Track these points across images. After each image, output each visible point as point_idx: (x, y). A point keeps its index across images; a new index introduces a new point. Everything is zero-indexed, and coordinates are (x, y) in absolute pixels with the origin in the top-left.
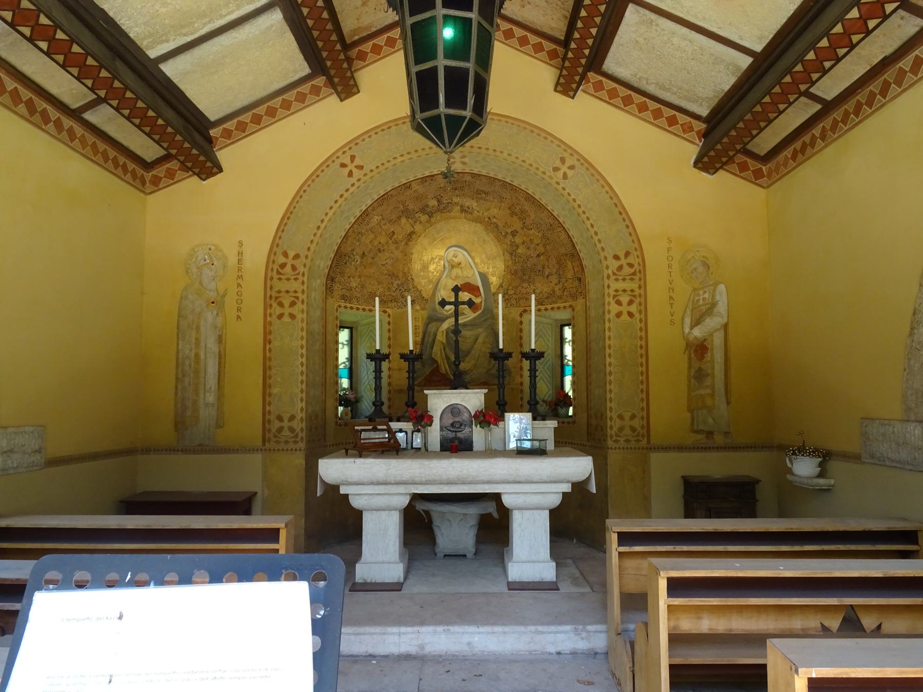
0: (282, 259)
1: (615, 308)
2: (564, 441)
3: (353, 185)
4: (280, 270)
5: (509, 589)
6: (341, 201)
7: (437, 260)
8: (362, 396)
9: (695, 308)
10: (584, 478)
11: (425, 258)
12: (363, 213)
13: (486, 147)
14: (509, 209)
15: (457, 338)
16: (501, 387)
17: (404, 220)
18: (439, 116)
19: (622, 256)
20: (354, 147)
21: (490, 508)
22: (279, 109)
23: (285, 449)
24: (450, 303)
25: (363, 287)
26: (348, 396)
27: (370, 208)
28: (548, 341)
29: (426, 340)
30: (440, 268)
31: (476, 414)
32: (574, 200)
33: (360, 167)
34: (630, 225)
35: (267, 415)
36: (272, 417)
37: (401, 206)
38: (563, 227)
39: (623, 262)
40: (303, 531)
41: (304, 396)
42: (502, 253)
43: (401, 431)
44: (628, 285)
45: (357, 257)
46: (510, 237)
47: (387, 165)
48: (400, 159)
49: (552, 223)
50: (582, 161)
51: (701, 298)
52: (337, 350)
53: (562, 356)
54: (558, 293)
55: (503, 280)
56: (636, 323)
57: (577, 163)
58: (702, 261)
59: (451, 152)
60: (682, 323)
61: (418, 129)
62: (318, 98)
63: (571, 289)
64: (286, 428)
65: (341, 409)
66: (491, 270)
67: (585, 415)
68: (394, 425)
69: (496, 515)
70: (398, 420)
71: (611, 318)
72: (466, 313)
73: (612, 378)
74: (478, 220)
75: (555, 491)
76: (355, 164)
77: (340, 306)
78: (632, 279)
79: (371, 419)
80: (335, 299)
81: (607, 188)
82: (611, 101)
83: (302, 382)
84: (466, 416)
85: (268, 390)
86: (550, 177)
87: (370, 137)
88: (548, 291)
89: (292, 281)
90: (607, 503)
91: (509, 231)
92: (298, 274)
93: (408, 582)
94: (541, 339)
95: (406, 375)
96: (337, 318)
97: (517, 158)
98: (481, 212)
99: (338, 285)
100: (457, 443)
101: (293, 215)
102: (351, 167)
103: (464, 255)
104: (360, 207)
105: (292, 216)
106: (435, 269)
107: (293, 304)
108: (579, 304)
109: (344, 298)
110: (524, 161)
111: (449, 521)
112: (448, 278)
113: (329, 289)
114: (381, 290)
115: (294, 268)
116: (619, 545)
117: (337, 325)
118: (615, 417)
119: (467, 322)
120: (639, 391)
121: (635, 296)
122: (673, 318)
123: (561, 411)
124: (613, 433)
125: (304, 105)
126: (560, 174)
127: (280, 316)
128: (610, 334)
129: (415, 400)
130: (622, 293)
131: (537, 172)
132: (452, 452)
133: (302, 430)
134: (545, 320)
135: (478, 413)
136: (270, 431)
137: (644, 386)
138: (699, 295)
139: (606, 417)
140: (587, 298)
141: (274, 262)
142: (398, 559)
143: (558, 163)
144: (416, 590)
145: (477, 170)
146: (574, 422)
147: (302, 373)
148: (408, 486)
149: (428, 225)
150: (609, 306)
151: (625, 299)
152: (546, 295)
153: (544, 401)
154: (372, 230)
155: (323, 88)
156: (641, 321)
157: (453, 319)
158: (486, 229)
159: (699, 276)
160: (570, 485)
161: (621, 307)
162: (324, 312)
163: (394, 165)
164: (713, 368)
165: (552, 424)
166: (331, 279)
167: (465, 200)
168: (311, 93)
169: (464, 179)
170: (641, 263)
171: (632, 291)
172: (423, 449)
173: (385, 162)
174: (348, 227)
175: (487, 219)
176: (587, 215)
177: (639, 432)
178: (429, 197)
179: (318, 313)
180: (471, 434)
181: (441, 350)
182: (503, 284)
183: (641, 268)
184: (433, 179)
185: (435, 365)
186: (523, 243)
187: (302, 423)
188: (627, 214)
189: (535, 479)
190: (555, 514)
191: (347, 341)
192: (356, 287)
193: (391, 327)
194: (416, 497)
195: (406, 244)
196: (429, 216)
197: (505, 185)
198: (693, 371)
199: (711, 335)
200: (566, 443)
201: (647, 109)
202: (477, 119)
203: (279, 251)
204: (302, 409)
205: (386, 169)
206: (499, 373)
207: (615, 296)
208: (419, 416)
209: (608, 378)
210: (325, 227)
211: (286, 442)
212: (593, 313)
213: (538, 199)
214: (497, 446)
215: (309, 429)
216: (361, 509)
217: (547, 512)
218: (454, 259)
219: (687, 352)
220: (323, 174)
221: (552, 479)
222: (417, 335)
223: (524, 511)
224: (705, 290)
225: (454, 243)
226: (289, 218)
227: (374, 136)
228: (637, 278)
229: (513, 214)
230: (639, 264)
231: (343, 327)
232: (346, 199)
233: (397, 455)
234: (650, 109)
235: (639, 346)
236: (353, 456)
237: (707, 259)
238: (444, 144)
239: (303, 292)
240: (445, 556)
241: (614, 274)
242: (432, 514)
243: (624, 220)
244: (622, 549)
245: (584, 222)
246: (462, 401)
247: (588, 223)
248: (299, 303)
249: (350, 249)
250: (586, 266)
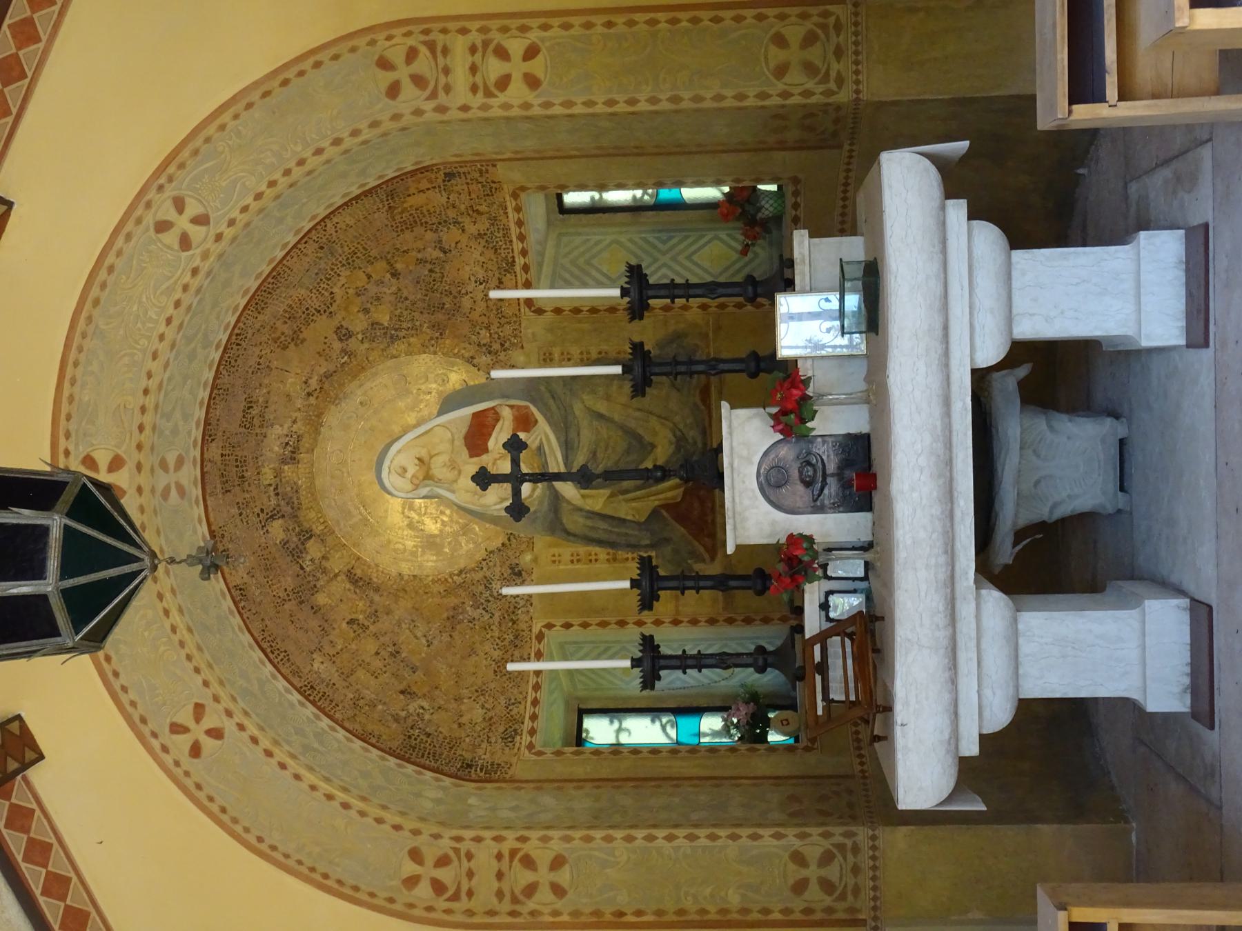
0: (424, 891)
1: (517, 92)
2: (841, 203)
3: (241, 727)
4: (450, 893)
5: (1206, 345)
6: (280, 755)
7: (413, 515)
8: (742, 686)
10: (933, 170)
11: (410, 544)
12: (307, 698)
13: (137, 411)
14: (285, 348)
15: (598, 476)
16: (714, 366)
17: (321, 599)
18: (66, 594)
19: (387, 77)
20: (152, 725)
21: (1007, 386)
22: (68, 902)
23: (871, 873)
24: (516, 493)
25: (481, 692)
26: (744, 721)
27: (296, 681)
28: (597, 244)
29: (604, 536)
30: (432, 505)
31: (781, 432)
32: (259, 196)
33: (199, 710)
34: (312, 59)
35: (792, 917)
36: (798, 904)
37: (287, 606)
38: (323, 220)
39: (403, 73)
40: (1068, 828)
41: (744, 832)
42: (390, 363)
43: (825, 606)
44: (460, 61)
45: (413, 707)
46: (353, 344)
47: (191, 648)
48: (176, 617)
49: (316, 245)
50: (162, 180)
52: (636, 750)
53: (635, 209)
54: (483, 225)
55: (455, 355)
57: (170, 192)
59: (153, 555)
61: (97, 639)
62: (38, 813)
63: (473, 196)
64: (823, 872)
65: (774, 737)
66: (434, 386)
67: (778, 155)
68: (813, 623)
69: (1023, 371)
70: (799, 611)
71: (540, 101)
72: (537, 443)
73: (686, 95)
74: (315, 422)
75: (965, 238)
76: (190, 723)
77: (530, 747)
78: (445, 51)
79: (799, 676)
80: (514, 760)
81: (226, 117)
82: (14, 111)
83: (713, 837)
84: (787, 453)
85: (736, 916)
86: (205, 256)
87: (124, 689)
88: (480, 248)
89: (473, 864)
90: (990, 100)
91: (337, 345)
92: (457, 851)
93: (1190, 587)
94: (595, 262)
95: (690, 593)
96: (558, 753)
97: (162, 337)
98: (294, 415)
99: (480, 752)
100: (851, 474)
101: (317, 866)
102: (198, 732)
103: (399, 452)
104: (292, 705)
105: (321, 868)
106: (435, 519)
107: (528, 862)
108: (509, 175)
109: (509, 737)
110: (169, 321)
111: (1037, 483)
112: (455, 486)
113: (491, 775)
114: (487, 647)
115: (443, 862)
116: (1100, 98)
117: (576, 753)
118: (780, 86)
119: (558, 439)
121: (486, 44)
123: (768, 209)
124: (821, 88)
125: (56, 845)
126: (196, 232)
127: (558, 890)
129: (750, 572)
130: (479, 76)
131: (192, 290)
132: (875, 488)
133: (826, 835)
134: (550, 252)
135: (780, 427)
136: (829, 910)
137: (705, 15)
139: (783, 106)
140: (495, 157)
141: (430, 909)
142: (1135, 613)
143: (171, 238)
144: (1209, 571)
145: (194, 430)
146: (796, 180)
147: (691, 838)
148: (958, 595)
149: (329, 540)
150: (512, 106)
151: (494, 68)
152: (490, 254)
153: (744, 252)
154: (347, 675)
155: (13, 800)
156: (545, 27)
157: (558, 485)
158: (336, 400)
160: (950, 202)
162: (545, 785)
163: (190, 630)
165: (801, 242)
166: (465, 771)
167: (268, 454)
168: (26, 830)
169: (218, 458)
171: (473, 50)
172: (869, 556)
173: (183, 653)
174: (341, 734)
175: (312, 400)
176: (292, 164)
178: (263, 540)
179: (548, 800)
180: (830, 440)
181: (627, 501)
182: (467, 355)
183: (416, 29)
184: (218, 534)
185: (665, 513)
186: (366, 311)
187: (810, 835)
188: (286, 66)
189: (939, 290)
190: (1019, 239)
191: (612, 722)
192: (483, 706)
193: (576, 621)
194: (987, 571)
195: (377, 590)
196: (311, 537)
197: (227, 361)
200: (845, 199)
201: (28, 23)
202: (68, 496)
203: (404, 896)
204: (778, 836)
205: (199, 649)
206: (680, 373)
207: (488, 94)
208: (791, 568)
209: (685, 105)
210: (345, 790)
211: (856, 870)
212: (530, 144)
213: (260, 281)
214: (858, 384)
215: (824, 816)
216: (1016, 704)
217: (1019, 256)
218: (409, 475)
220: (217, 798)
221: (938, 248)
222: (593, 558)
223: (1015, 311)
225: (371, 476)
226: (326, 876)
227: (123, 680)
228: (440, 39)
229: (297, 338)
231: (579, 739)
232: (276, 743)
233: (882, 618)
234: (28, 13)
235: (606, 30)
236: (889, 724)
238: (135, 575)
239: (498, 839)
240: (1122, 489)
241: (434, 95)
242: (1022, 522)
243: (301, 74)
244: (1112, 92)
245: (309, 173)
246: (751, 463)
247: (313, 162)
248: (527, 848)
249: (394, 725)
250: (417, 163)
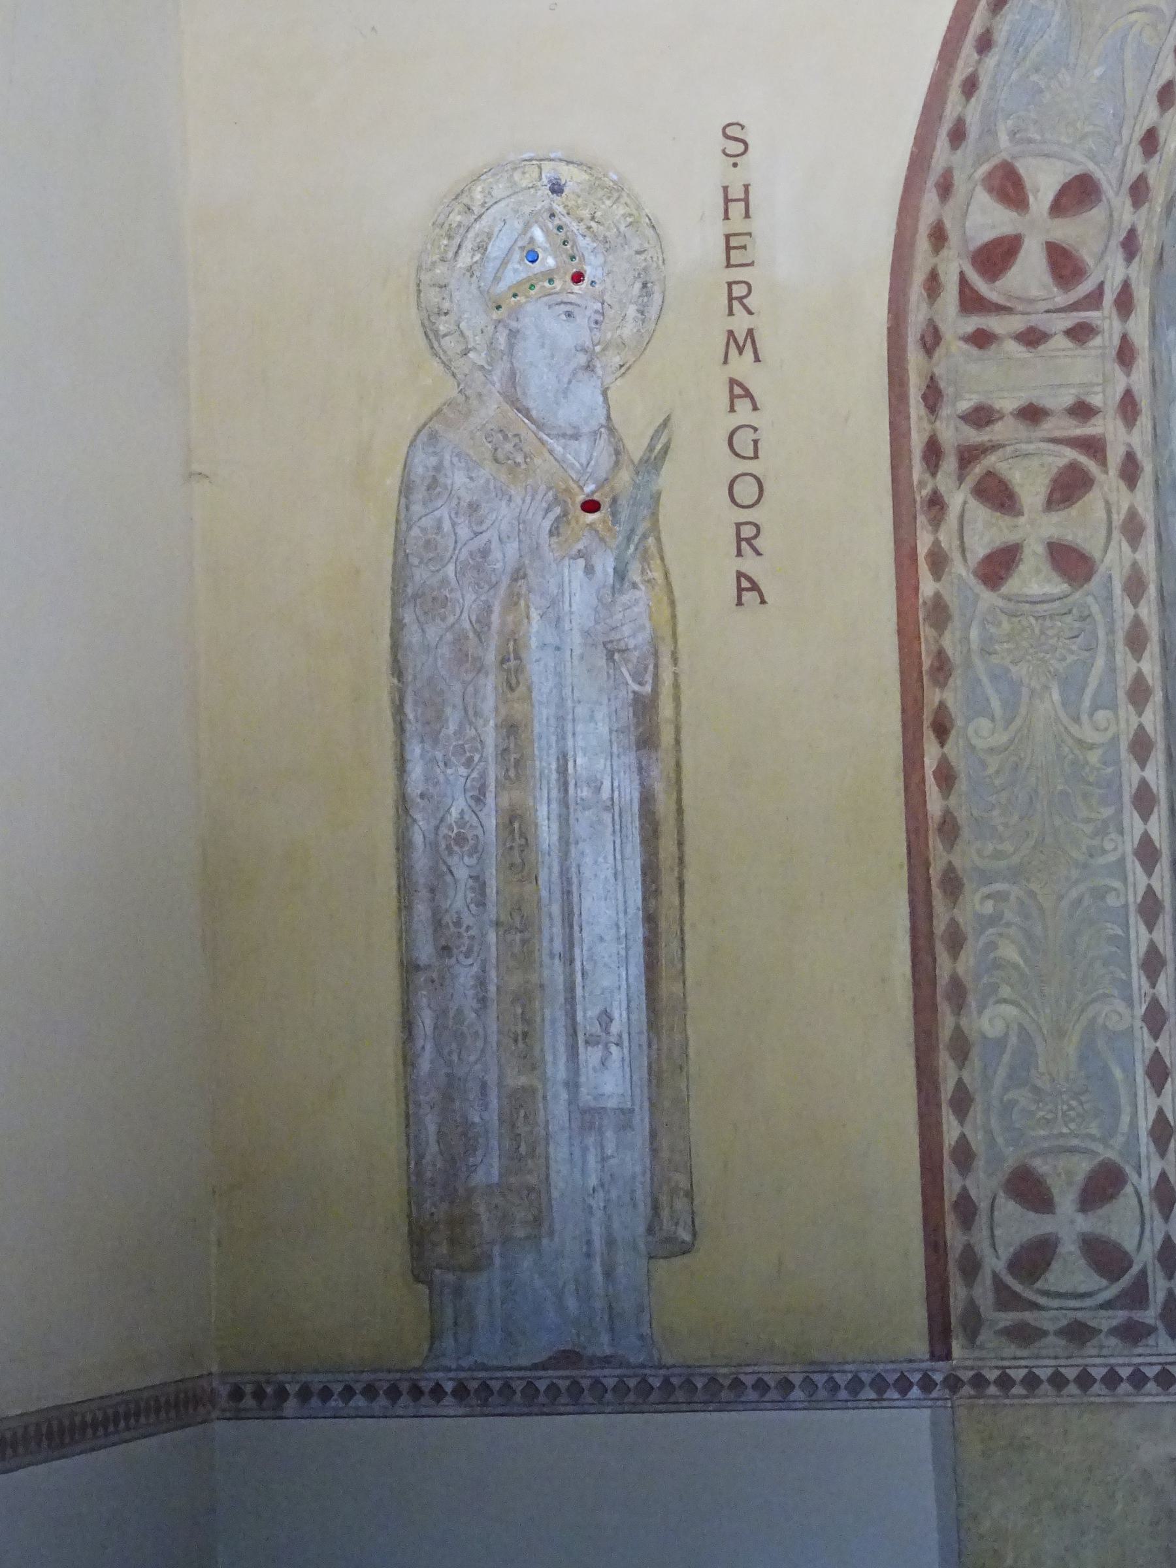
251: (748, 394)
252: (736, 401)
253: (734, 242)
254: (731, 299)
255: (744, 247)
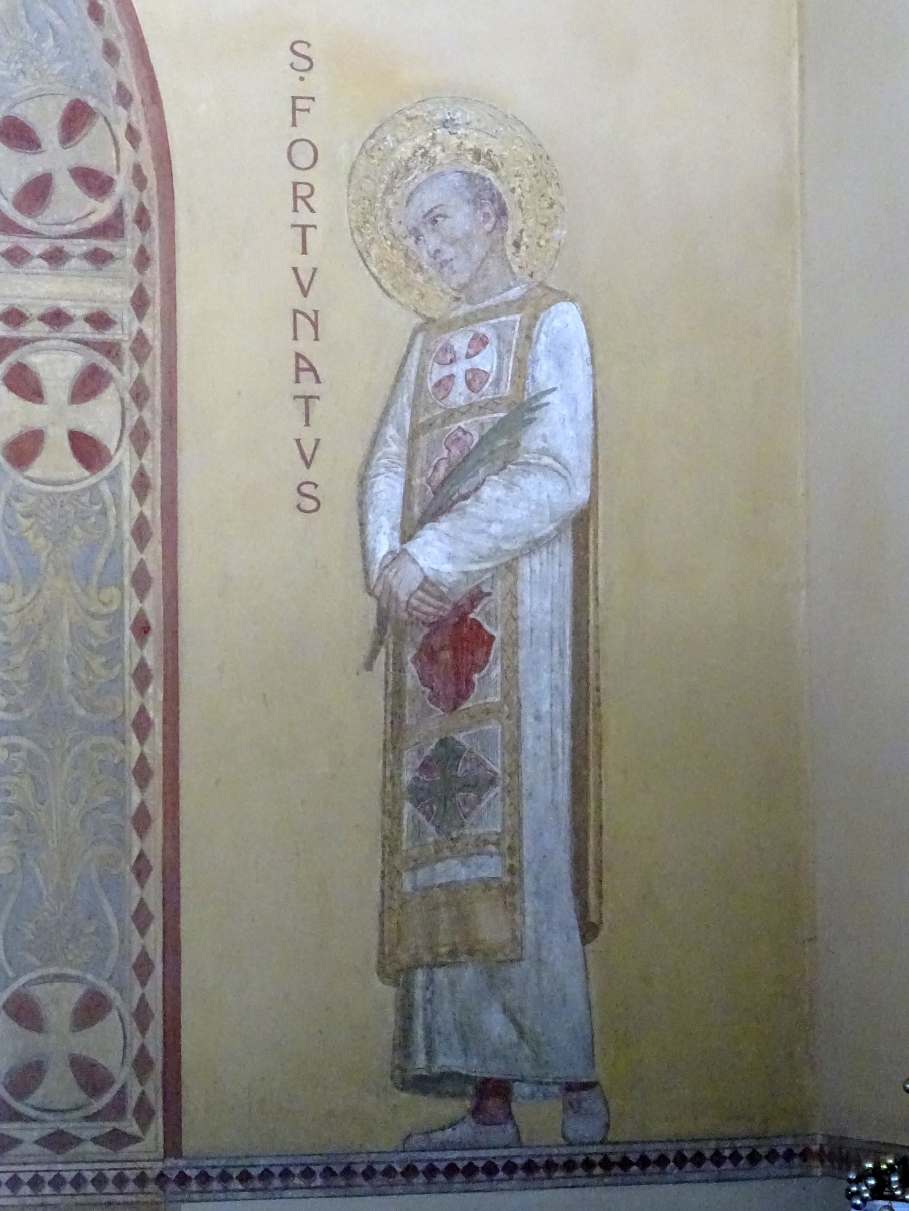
9: (430, 425)
51: (459, 369)
56: (117, 496)
58: (470, 178)
60: (361, 504)
78: (98, 258)
120: (127, 868)
121: (111, 350)
122: (312, 474)
128: (137, 556)
137: (154, 844)
138: (448, 356)
156: (141, 485)
159: (449, 252)
161: (73, 163)
164: (515, 747)
170: (150, 172)
171: (100, 320)
177: (122, 1094)
183: (151, 198)
198: (411, 758)
199: (510, 567)
219: (381, 657)
224: (482, 329)
230: (139, 179)
235: (128, 622)
237: (495, 169)
251: (312, 369)
252: (301, 373)
253: (300, 104)
254: (296, 197)
255: (308, 110)
